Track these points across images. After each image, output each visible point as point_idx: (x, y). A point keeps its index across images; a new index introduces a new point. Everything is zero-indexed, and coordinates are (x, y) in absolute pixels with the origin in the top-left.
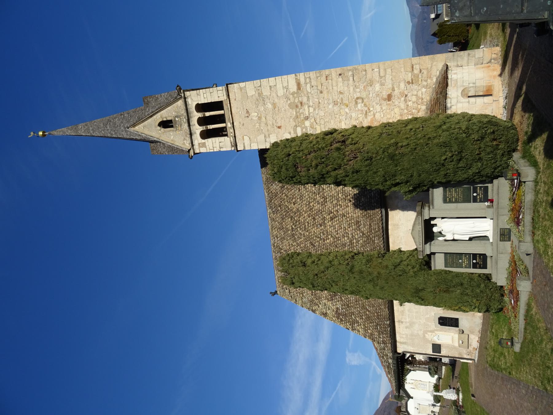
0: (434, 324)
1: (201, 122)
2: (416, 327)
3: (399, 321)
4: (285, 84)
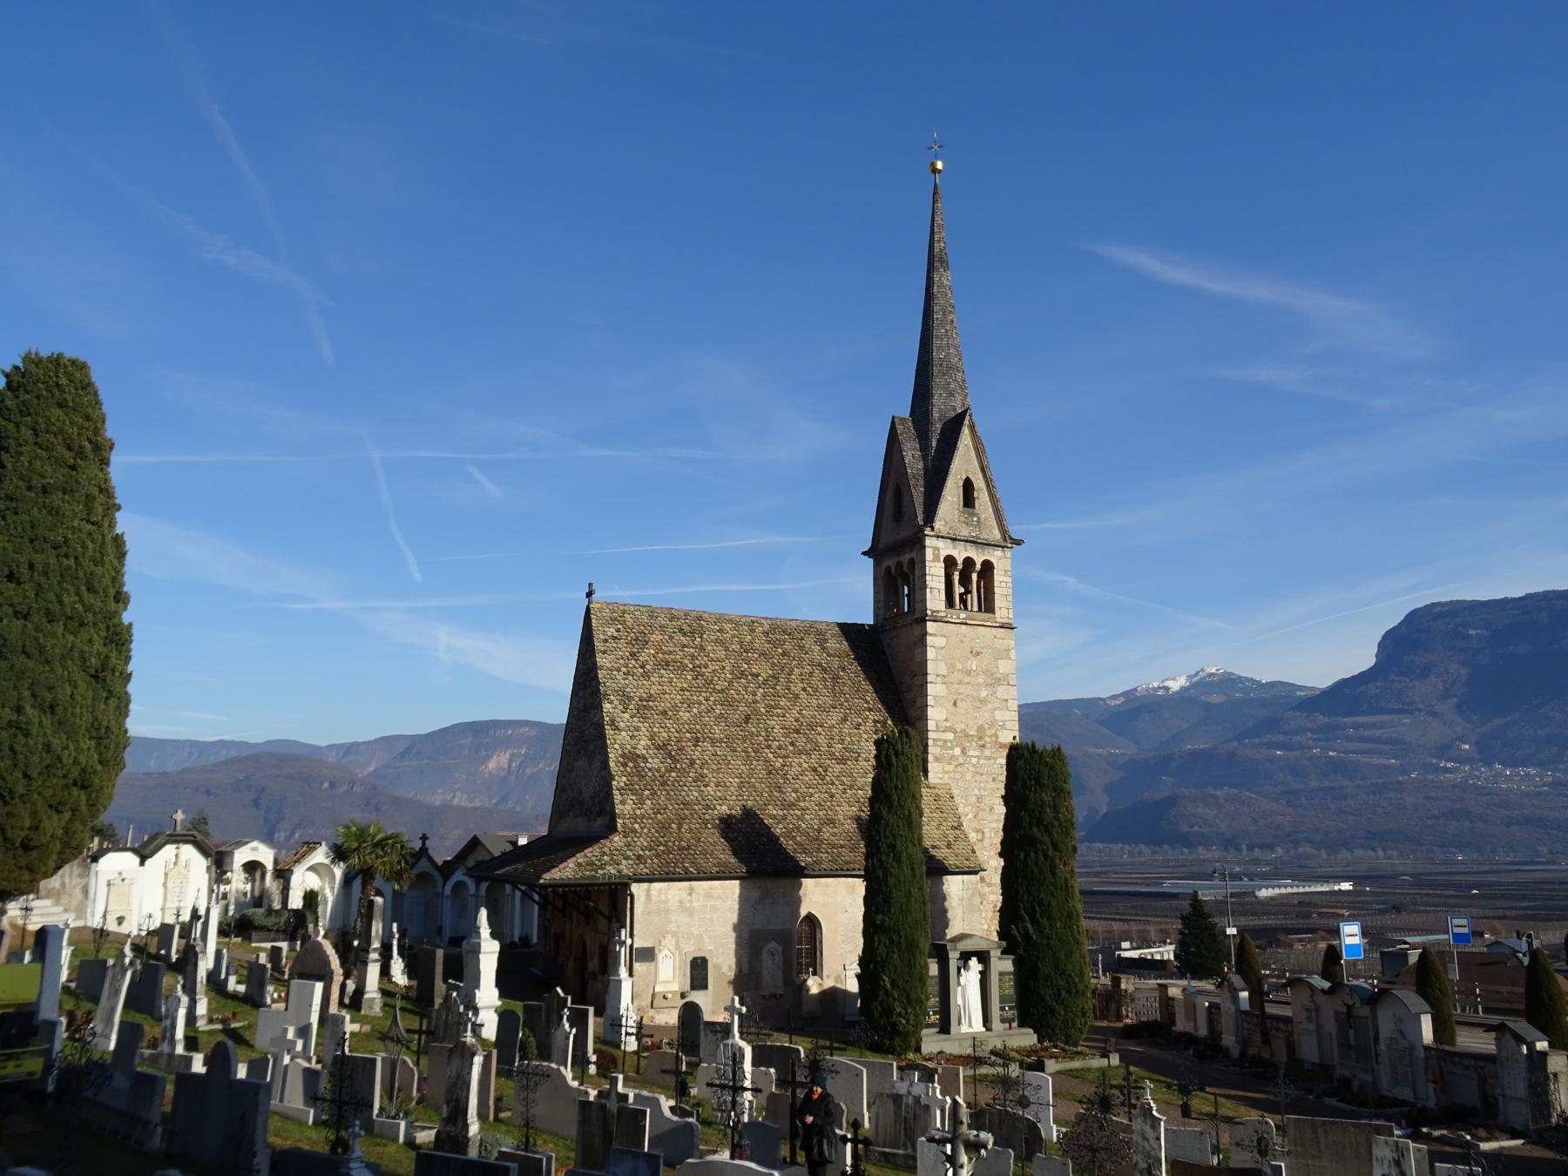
0: (692, 950)
1: (969, 562)
2: (684, 919)
3: (691, 889)
4: (1008, 725)
